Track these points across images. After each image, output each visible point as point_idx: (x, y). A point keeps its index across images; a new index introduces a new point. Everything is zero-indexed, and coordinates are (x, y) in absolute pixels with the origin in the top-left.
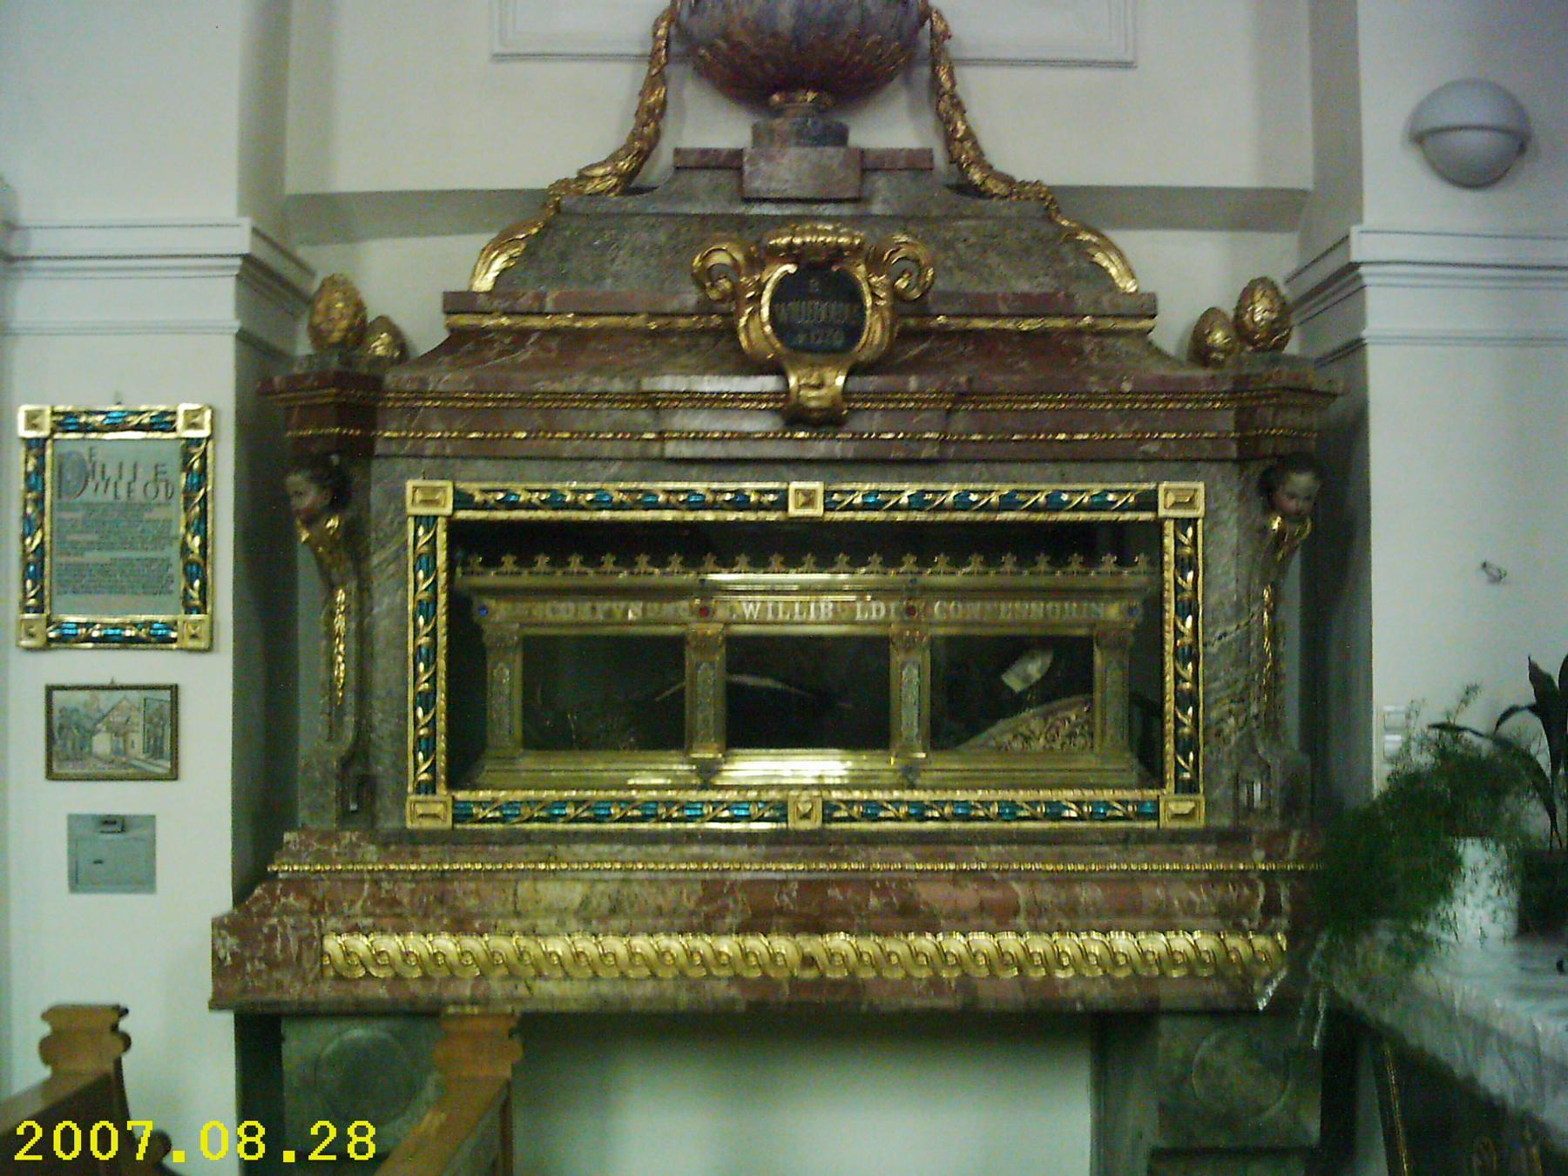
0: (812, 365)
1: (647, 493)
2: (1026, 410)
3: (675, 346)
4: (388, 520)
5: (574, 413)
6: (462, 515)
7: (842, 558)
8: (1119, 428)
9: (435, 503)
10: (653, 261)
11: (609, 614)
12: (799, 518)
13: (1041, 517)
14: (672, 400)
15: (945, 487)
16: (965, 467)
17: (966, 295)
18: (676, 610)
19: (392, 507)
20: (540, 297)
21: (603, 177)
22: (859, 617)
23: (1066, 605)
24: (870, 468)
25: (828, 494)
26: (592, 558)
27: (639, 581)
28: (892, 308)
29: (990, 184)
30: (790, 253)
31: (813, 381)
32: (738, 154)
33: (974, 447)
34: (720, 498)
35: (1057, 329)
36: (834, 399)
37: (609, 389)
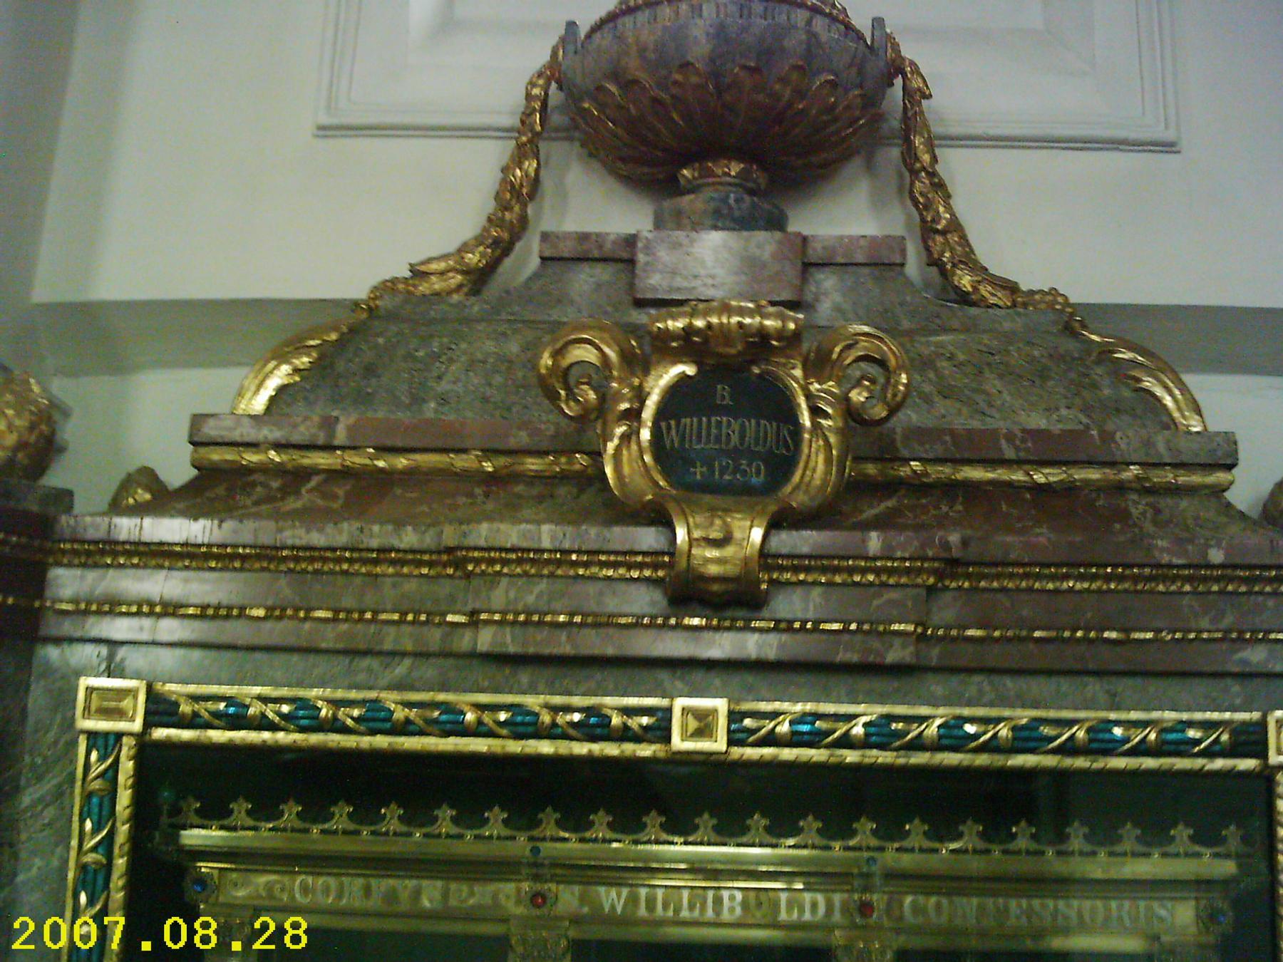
0: (713, 510)
1: (446, 707)
2: (1056, 592)
3: (519, 496)
4: (51, 737)
5: (341, 581)
6: (160, 733)
7: (758, 821)
8: (1204, 623)
9: (119, 714)
10: (498, 379)
11: (391, 897)
12: (688, 753)
13: (1081, 762)
14: (491, 562)
15: (924, 711)
16: (954, 680)
17: (952, 432)
18: (495, 896)
19: (58, 719)
20: (329, 424)
21: (442, 273)
22: (783, 916)
23: (1114, 904)
24: (801, 679)
25: (734, 717)
26: (524, 816)
27: (438, 848)
28: (842, 432)
29: (985, 290)
30: (689, 345)
31: (715, 534)
32: (630, 241)
33: (970, 648)
34: (562, 719)
35: (1086, 482)
36: (746, 561)
37: (396, 543)
